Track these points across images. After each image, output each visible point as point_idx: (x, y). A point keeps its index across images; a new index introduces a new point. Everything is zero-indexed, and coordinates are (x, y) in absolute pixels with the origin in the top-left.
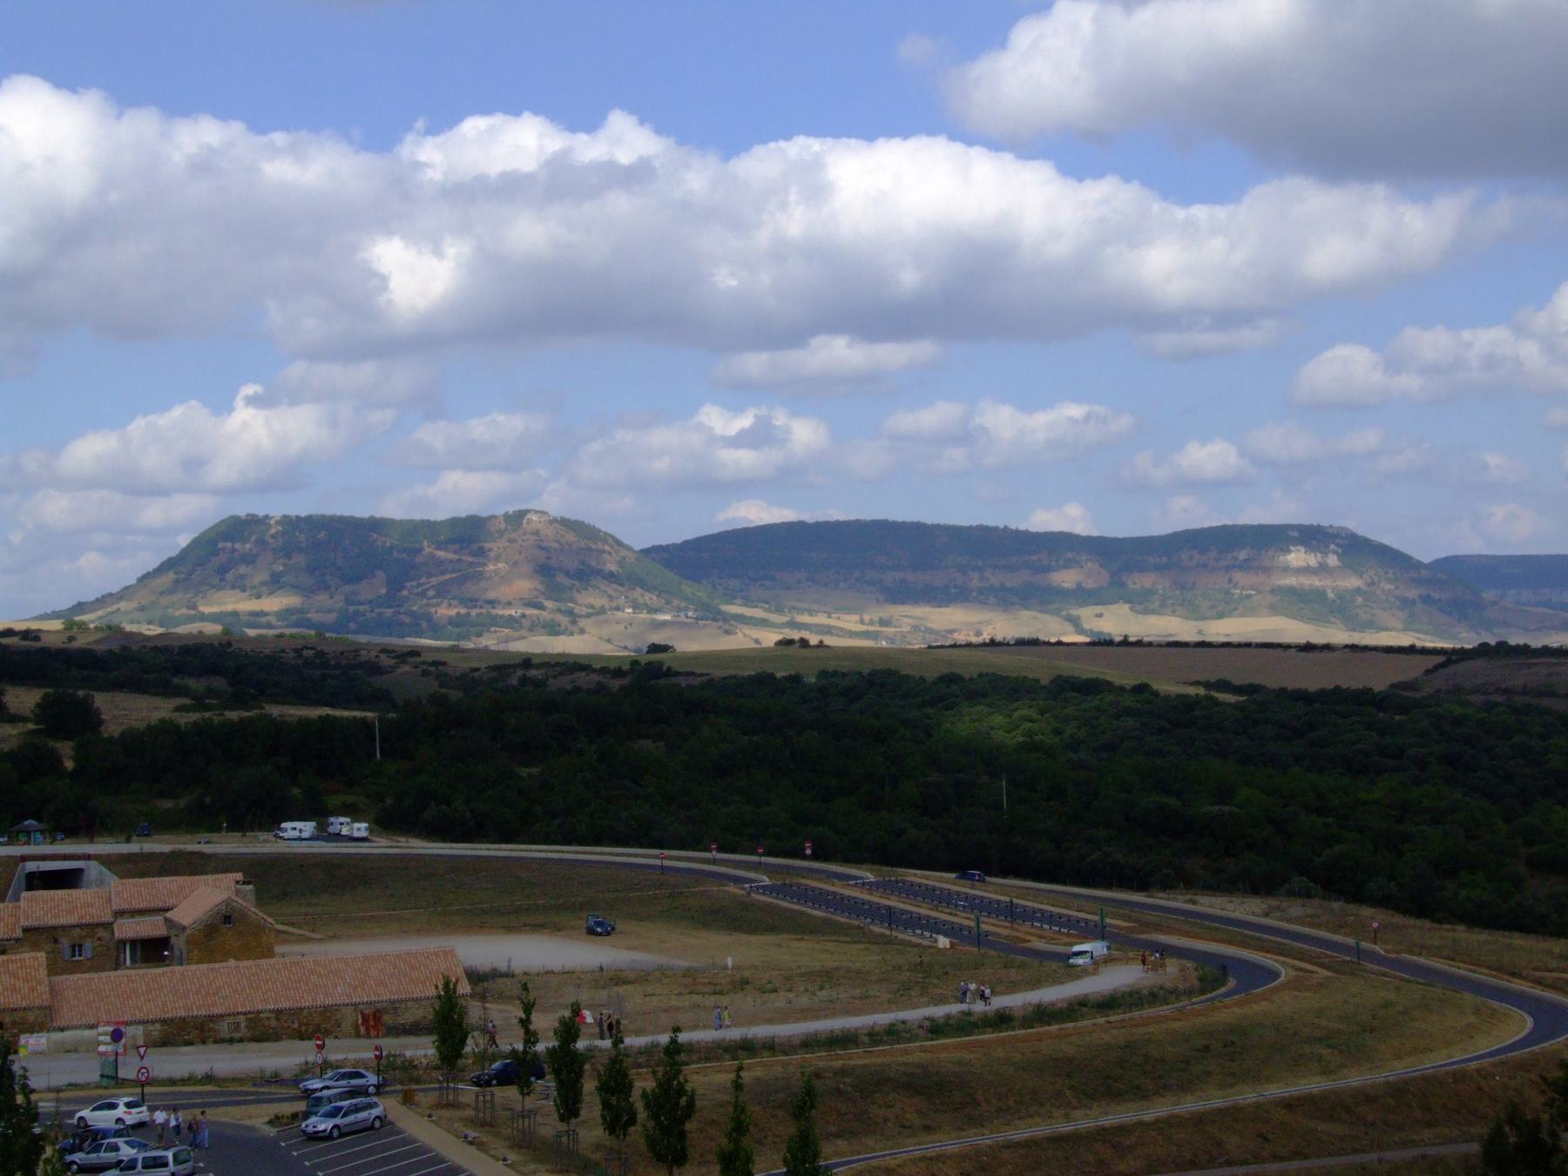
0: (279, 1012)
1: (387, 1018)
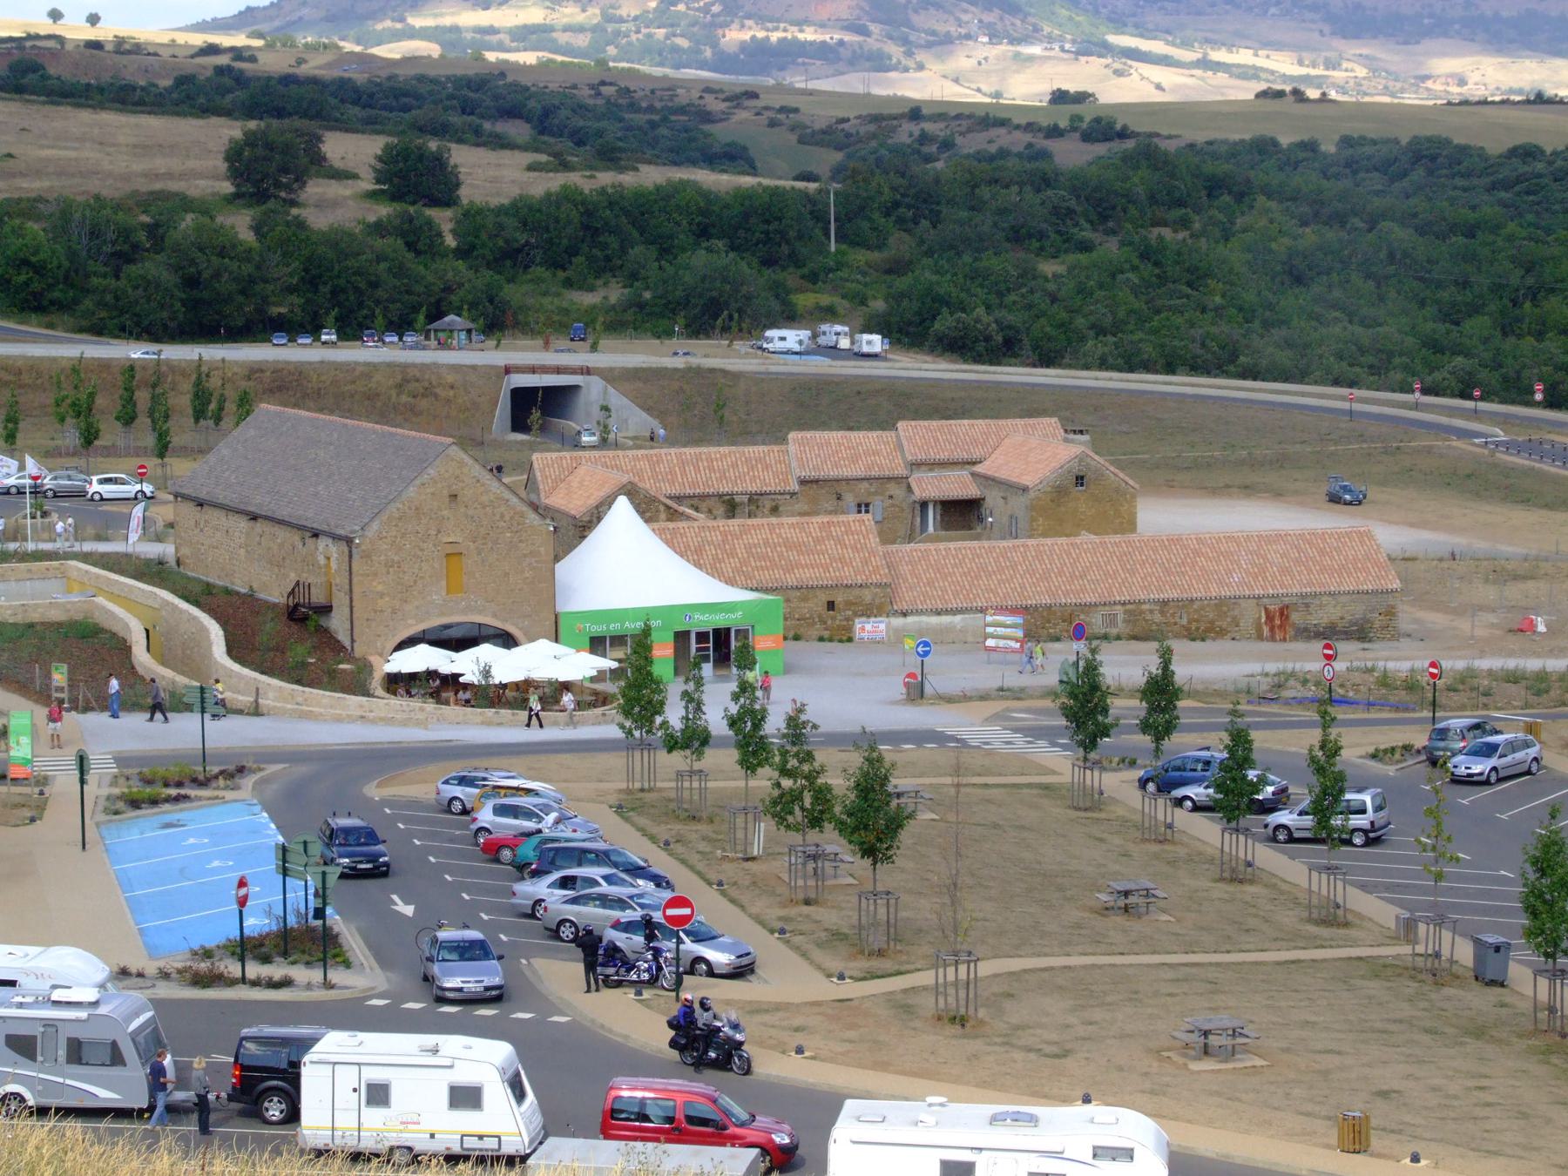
0: (1165, 603)
1: (1295, 617)
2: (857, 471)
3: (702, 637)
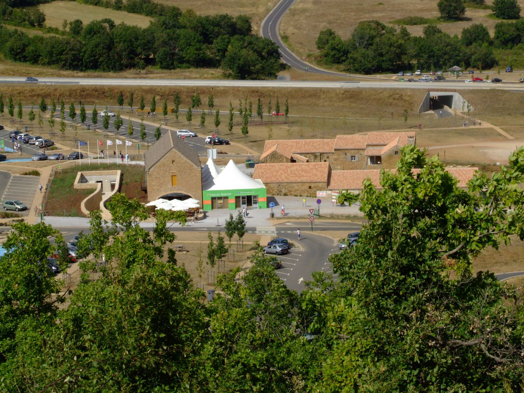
2: (352, 147)
3: (243, 198)
